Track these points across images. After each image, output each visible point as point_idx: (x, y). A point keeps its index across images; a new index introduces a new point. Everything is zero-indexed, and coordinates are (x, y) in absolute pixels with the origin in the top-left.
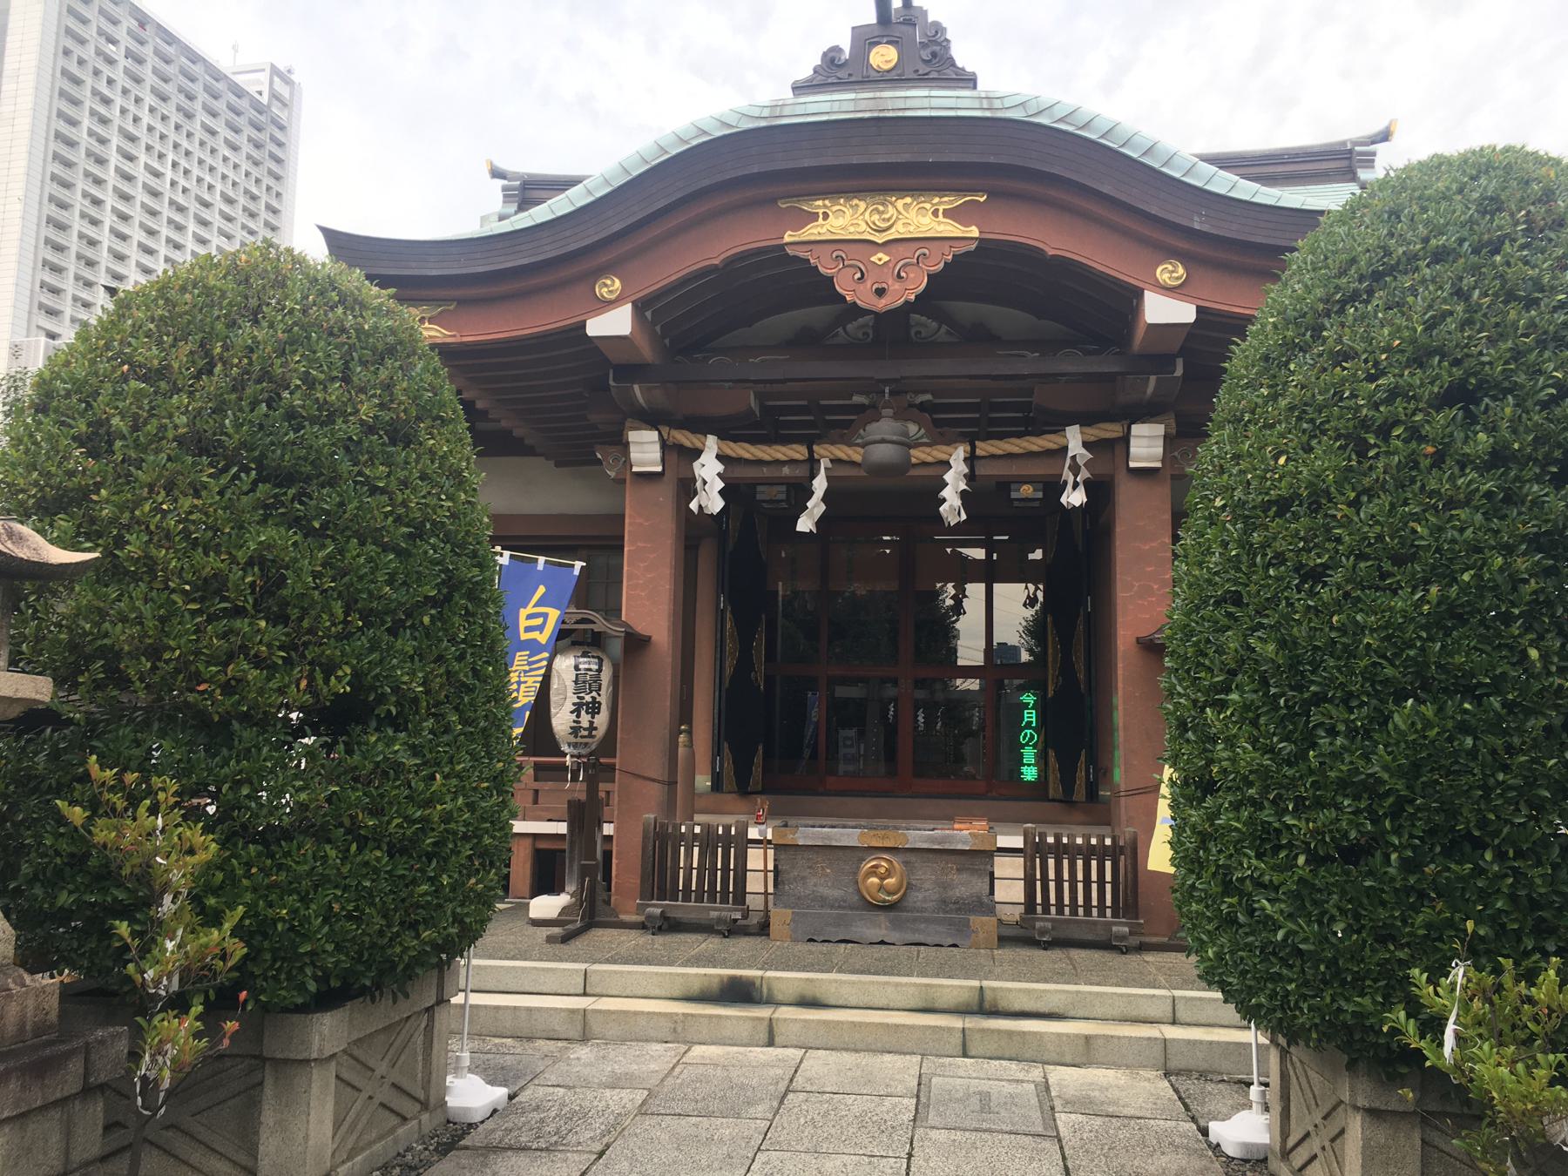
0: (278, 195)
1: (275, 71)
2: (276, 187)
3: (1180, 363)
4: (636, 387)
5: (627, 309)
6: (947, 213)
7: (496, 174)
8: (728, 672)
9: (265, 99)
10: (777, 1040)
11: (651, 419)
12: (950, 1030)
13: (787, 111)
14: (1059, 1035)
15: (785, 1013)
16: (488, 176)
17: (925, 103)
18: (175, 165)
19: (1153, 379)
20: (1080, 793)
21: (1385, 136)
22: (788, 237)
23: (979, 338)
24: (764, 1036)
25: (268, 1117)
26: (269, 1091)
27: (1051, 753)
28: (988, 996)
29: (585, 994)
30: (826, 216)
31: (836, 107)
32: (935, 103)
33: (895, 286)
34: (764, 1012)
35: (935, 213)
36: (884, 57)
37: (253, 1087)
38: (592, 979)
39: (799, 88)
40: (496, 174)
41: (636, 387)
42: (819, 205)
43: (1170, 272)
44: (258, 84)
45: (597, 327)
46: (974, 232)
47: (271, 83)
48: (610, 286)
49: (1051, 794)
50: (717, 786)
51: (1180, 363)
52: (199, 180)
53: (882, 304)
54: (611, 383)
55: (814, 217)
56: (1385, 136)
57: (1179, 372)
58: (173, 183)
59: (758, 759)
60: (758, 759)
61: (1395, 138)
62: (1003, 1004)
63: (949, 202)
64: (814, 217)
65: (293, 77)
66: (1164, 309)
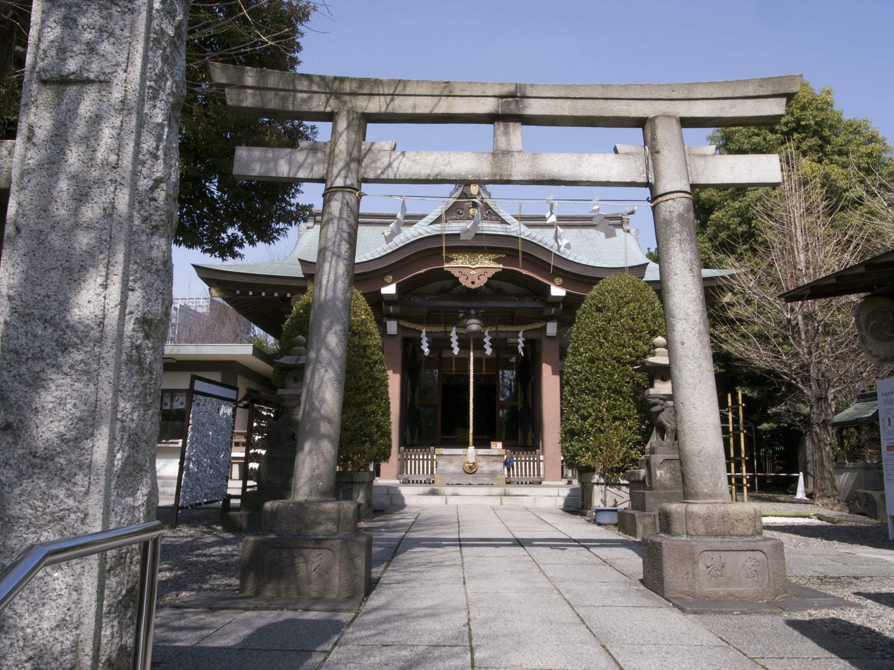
21: (632, 213)
33: (477, 281)
46: (501, 266)
48: (389, 278)
53: (473, 287)
56: (632, 213)
63: (493, 256)
66: (557, 291)
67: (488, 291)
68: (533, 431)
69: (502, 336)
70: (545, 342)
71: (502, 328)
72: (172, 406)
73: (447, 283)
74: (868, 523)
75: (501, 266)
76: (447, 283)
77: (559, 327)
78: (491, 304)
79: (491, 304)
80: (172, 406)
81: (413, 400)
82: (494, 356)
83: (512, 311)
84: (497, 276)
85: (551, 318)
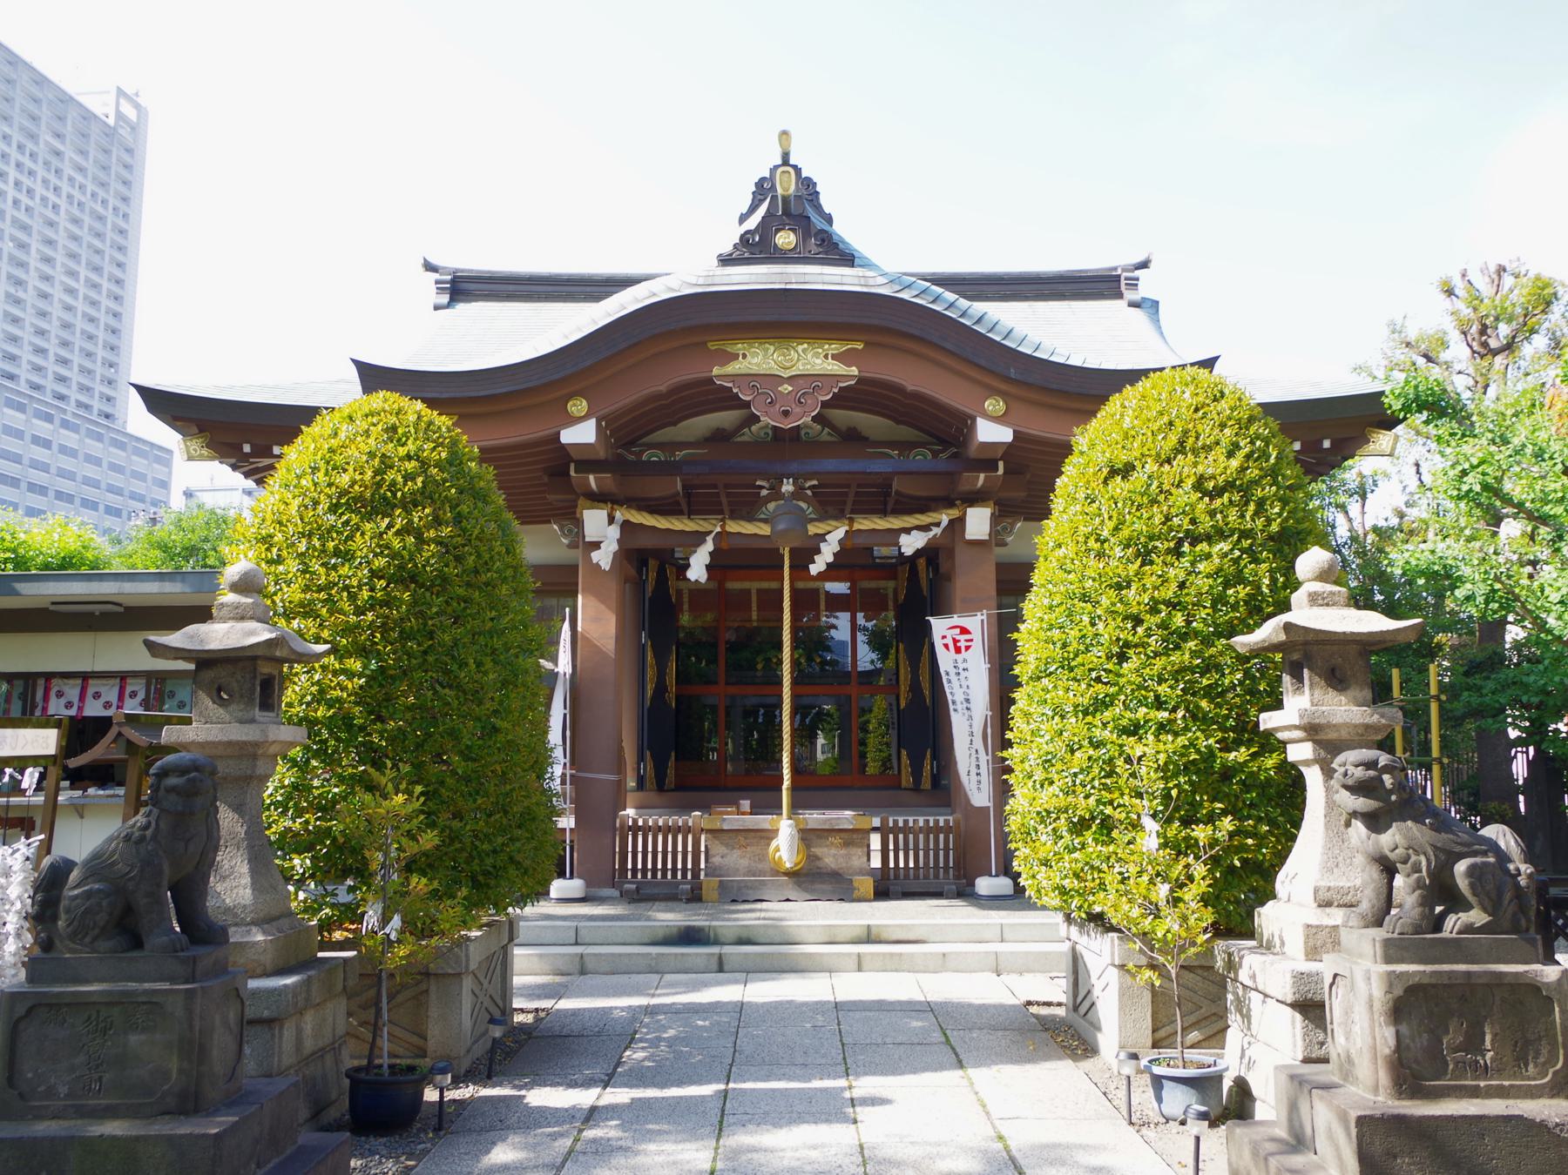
0: (125, 216)
1: (121, 93)
2: (123, 207)
3: (1001, 464)
4: (591, 477)
5: (592, 423)
6: (834, 357)
7: (429, 267)
8: (649, 693)
9: (111, 121)
10: (726, 968)
11: (598, 499)
12: (849, 955)
13: (717, 280)
14: (925, 954)
15: (727, 949)
16: (422, 269)
17: (819, 279)
18: (17, 184)
19: (982, 476)
20: (926, 783)
21: (1144, 265)
22: (716, 371)
23: (852, 437)
24: (715, 966)
25: (434, 1012)
26: (433, 996)
27: (904, 753)
28: (874, 931)
29: (577, 944)
30: (744, 356)
31: (753, 278)
32: (827, 278)
34: (715, 950)
35: (826, 357)
36: (786, 239)
37: (421, 993)
38: (582, 933)
39: (726, 261)
40: (429, 267)
41: (591, 477)
42: (739, 347)
43: (994, 405)
44: (101, 106)
45: (569, 436)
46: (854, 371)
47: (118, 104)
48: (578, 406)
49: (904, 784)
50: (641, 785)
51: (1001, 464)
52: (44, 199)
54: (572, 473)
55: (736, 357)
56: (1144, 265)
57: (1001, 471)
58: (16, 202)
59: (672, 763)
60: (672, 763)
61: (1152, 265)
62: (885, 936)
63: (835, 347)
64: (735, 357)
65: (139, 100)
66: (991, 432)
67: (826, 435)
68: (934, 757)
69: (861, 541)
70: (962, 556)
71: (865, 524)
72: (80, 709)
73: (724, 418)
74: (1507, 844)
75: (854, 371)
76: (724, 418)
77: (995, 520)
78: (830, 464)
79: (830, 464)
80: (80, 709)
81: (661, 689)
82: (972, 452)
83: (884, 484)
84: (847, 397)
85: (974, 499)
